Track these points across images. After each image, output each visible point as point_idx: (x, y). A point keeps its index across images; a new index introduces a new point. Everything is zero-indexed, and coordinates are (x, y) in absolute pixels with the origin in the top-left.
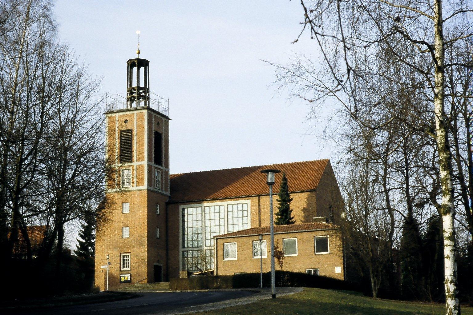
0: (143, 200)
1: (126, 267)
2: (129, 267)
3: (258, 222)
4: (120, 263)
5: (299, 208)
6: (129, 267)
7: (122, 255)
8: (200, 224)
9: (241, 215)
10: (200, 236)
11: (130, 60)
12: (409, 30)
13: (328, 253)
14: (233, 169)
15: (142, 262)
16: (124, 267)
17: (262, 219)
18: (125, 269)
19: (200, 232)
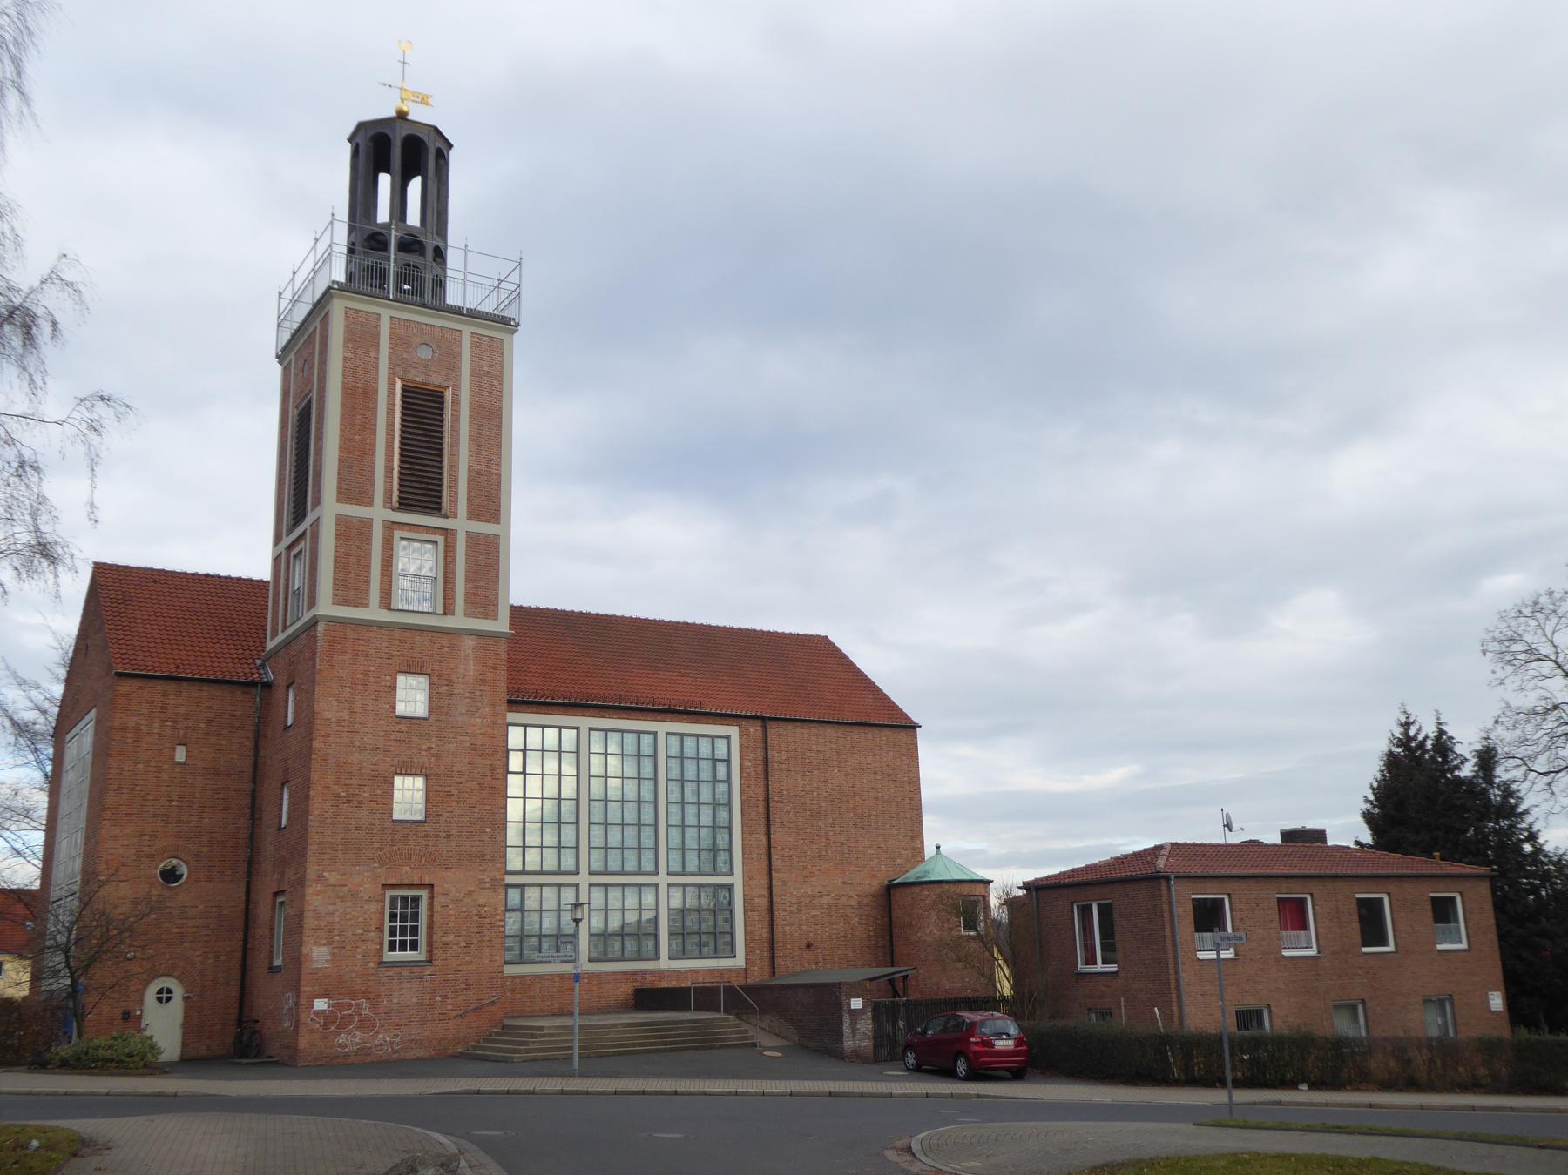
0: (489, 676)
1: (403, 948)
2: (414, 946)
3: (762, 804)
4: (430, 927)
5: (875, 773)
6: (414, 946)
7: (424, 893)
8: (569, 789)
9: (706, 775)
10: (647, 833)
11: (361, 126)
12: (94, 443)
13: (1391, 948)
14: (660, 621)
15: (480, 926)
16: (392, 947)
17: (774, 797)
18: (398, 955)
19: (567, 816)
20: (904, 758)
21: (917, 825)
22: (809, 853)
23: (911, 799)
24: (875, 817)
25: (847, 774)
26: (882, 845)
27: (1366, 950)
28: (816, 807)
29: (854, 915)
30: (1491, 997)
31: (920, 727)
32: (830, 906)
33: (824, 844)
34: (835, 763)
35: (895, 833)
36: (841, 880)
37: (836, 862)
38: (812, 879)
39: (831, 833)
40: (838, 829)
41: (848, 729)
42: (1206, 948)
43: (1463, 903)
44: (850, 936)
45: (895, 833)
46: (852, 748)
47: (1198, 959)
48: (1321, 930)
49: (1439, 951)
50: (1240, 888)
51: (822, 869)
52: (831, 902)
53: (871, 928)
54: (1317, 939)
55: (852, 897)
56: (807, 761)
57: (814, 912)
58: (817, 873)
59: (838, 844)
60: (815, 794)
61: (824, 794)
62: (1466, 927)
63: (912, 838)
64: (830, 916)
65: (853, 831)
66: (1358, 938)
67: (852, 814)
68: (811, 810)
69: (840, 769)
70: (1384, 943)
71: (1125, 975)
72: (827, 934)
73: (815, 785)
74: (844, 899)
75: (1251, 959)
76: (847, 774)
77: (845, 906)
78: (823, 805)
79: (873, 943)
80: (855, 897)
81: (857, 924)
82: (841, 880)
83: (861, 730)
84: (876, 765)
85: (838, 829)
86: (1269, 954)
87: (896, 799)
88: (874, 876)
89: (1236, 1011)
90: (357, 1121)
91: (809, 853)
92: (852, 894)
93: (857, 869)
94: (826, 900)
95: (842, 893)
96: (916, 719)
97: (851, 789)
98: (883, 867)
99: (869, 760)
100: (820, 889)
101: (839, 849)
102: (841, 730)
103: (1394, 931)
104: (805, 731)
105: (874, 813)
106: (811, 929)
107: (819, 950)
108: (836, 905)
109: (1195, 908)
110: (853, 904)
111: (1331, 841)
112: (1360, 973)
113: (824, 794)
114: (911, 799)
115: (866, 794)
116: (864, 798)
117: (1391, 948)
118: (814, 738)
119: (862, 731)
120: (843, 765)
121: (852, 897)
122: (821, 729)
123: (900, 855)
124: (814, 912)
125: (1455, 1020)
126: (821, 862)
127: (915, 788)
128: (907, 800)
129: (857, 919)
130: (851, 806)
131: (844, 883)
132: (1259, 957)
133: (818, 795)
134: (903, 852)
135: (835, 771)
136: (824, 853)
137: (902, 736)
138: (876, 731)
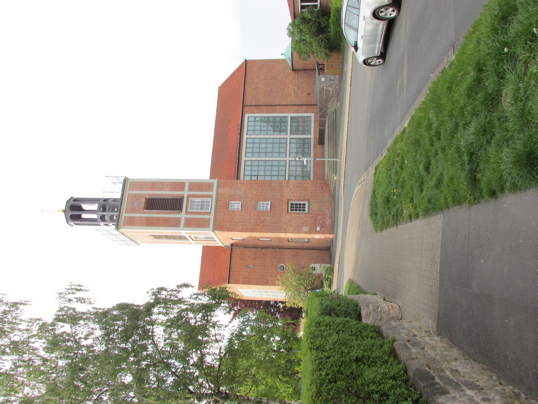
41: (246, 81)
69: (258, 84)
77: (298, 83)
83: (247, 77)
94: (296, 89)
102: (247, 83)
131: (291, 83)
137: (248, 64)
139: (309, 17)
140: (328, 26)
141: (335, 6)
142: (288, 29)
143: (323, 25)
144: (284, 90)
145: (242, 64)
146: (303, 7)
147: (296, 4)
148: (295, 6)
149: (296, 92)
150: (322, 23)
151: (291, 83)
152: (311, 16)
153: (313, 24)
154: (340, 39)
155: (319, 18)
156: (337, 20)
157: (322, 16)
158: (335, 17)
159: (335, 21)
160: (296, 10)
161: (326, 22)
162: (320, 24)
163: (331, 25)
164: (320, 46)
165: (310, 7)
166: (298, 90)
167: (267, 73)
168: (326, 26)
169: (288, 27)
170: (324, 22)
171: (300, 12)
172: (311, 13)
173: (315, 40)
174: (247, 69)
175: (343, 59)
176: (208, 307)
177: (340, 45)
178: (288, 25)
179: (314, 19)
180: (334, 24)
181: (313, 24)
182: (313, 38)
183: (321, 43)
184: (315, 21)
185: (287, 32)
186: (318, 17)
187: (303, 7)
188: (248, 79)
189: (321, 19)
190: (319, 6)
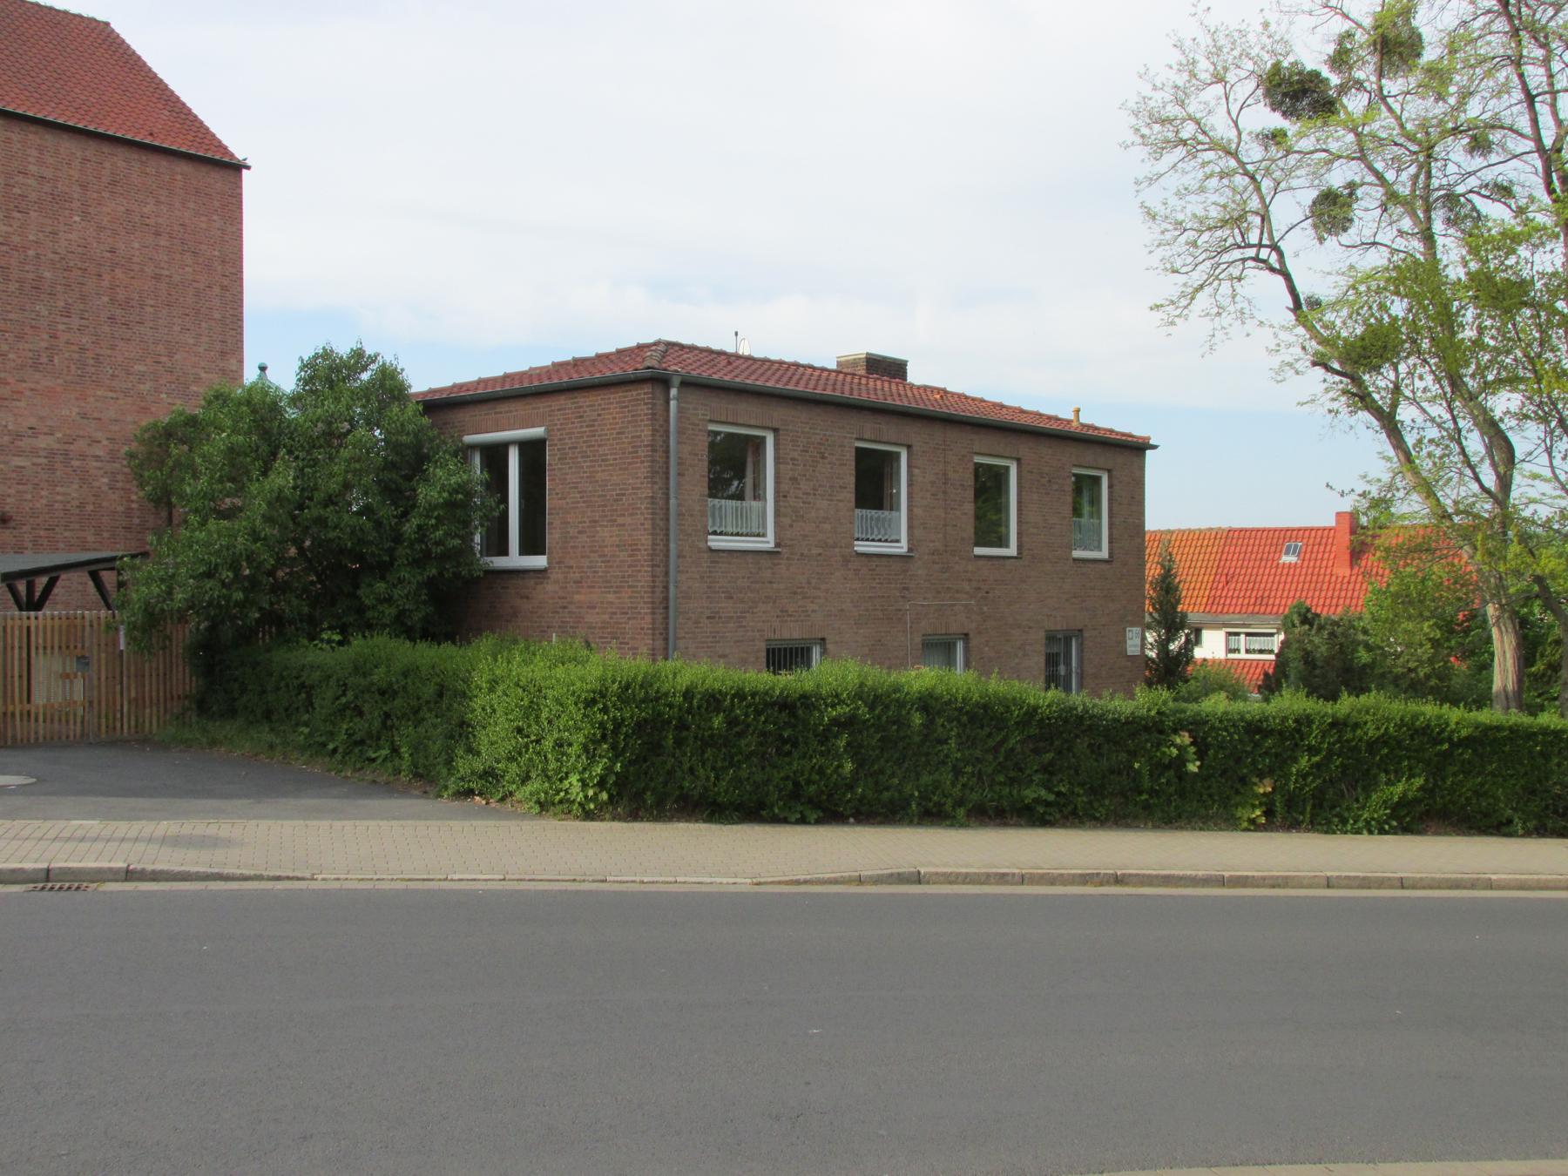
5: (157, 234)
20: (215, 217)
21: (233, 333)
22: (11, 356)
23: (224, 288)
24: (151, 310)
25: (100, 228)
26: (164, 359)
27: (979, 551)
28: (31, 276)
29: (101, 472)
30: (1129, 635)
31: (248, 168)
32: (51, 454)
33: (44, 344)
34: (76, 204)
35: (191, 341)
36: (77, 410)
37: (69, 378)
38: (18, 404)
39: (61, 327)
40: (75, 322)
41: (106, 148)
42: (729, 530)
43: (1110, 486)
44: (91, 507)
45: (191, 341)
46: (114, 183)
47: (711, 550)
48: (918, 511)
49: (1075, 560)
50: (798, 419)
51: (39, 387)
52: (56, 446)
53: (134, 497)
54: (910, 527)
55: (99, 442)
56: (17, 191)
57: (18, 461)
58: (28, 393)
59: (75, 348)
60: (31, 253)
61: (52, 256)
62: (1110, 528)
63: (223, 354)
64: (52, 470)
65: (106, 328)
66: (969, 530)
67: (106, 299)
68: (21, 281)
69: (85, 215)
70: (1002, 542)
71: (560, 576)
72: (44, 501)
73: (31, 238)
74: (81, 445)
75: (802, 554)
76: (100, 228)
77: (83, 457)
78: (47, 275)
79: (136, 521)
80: (105, 442)
81: (105, 488)
82: (77, 410)
83: (135, 155)
84: (160, 220)
85: (75, 322)
86: (834, 547)
87: (195, 285)
88: (145, 410)
89: (768, 650)
90: (1513, 487)
91: (11, 356)
92: (99, 435)
93: (111, 394)
94: (43, 442)
95: (81, 433)
96: (239, 154)
97: (108, 255)
98: (163, 396)
99: (145, 210)
100: (32, 422)
101: (76, 356)
102: (92, 149)
103: (1020, 522)
104: (15, 137)
105: (152, 302)
106: (12, 491)
107: (25, 529)
108: (66, 454)
109: (712, 445)
110: (100, 453)
111: (915, 376)
112: (967, 588)
113: (52, 256)
114: (224, 288)
115: (136, 268)
116: (132, 274)
117: (1012, 550)
118: (34, 153)
119: (136, 156)
120: (91, 210)
121: (99, 442)
122: (49, 139)
123: (197, 380)
124: (18, 461)
125: (1082, 670)
126: (37, 376)
127: (234, 271)
128: (217, 290)
129: (105, 480)
130: (106, 284)
131: (84, 416)
132: (815, 551)
133: (38, 256)
134: (203, 375)
135: (77, 219)
136: (44, 360)
137: (216, 179)
138: (163, 163)
139: (427, 494)
140: (357, 621)
141: (480, 679)
142: (359, 359)
143: (373, 590)
144: (36, 366)
145: (223, 148)
146: (495, 456)
147: (518, 409)
148: (503, 407)
149: (24, 443)
150: (381, 586)
151: (84, 416)
152: (433, 507)
153: (378, 524)
154: (268, 715)
155: (419, 562)
156: (382, 693)
157: (430, 583)
158: (405, 674)
159: (379, 676)
160: (479, 413)
161: (390, 611)
162: (382, 569)
163: (358, 645)
164: (209, 575)
165: (492, 502)
166: (35, 452)
167: (157, 277)
168: (361, 610)
169: (373, 359)
170: (389, 600)
171: (469, 439)
172: (457, 506)
173: (255, 536)
174: (183, 167)
175: (142, 741)
176: (814, 803)
177: (230, 713)
178: (387, 357)
179: (409, 527)
180: (359, 669)
181: (378, 524)
182: (268, 519)
183: (227, 575)
184: (398, 538)
185: (343, 349)
186: (427, 555)
187: (495, 456)
188: (120, 160)
189: (411, 578)
190: (499, 562)
